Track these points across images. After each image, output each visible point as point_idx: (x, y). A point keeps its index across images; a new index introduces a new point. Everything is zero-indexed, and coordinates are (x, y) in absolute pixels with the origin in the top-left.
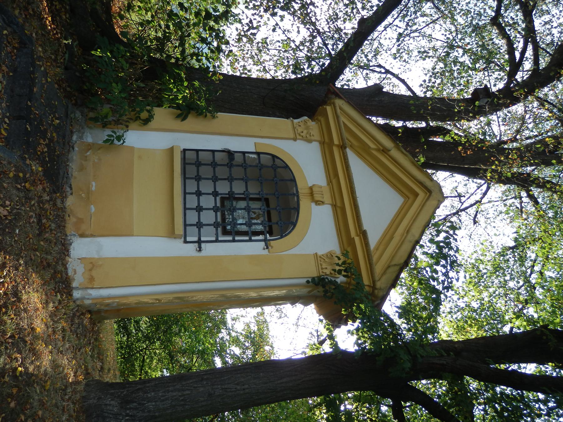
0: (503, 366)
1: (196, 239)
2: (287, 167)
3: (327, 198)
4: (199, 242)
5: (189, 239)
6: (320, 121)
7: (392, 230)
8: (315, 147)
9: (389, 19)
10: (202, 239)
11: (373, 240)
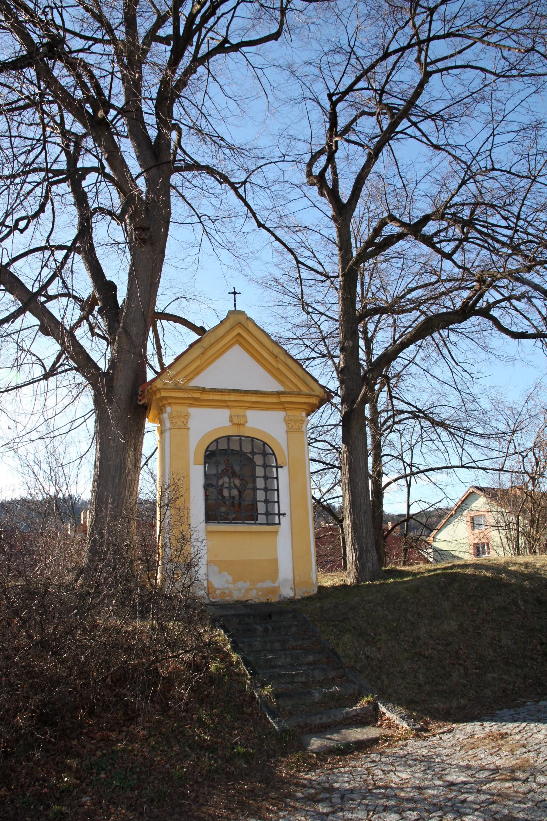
0: (359, 399)
1: (277, 517)
2: (216, 441)
3: (239, 412)
4: (279, 515)
5: (277, 522)
6: (166, 398)
7: (269, 366)
8: (194, 411)
9: (47, 279)
10: (277, 512)
11: (281, 389)
